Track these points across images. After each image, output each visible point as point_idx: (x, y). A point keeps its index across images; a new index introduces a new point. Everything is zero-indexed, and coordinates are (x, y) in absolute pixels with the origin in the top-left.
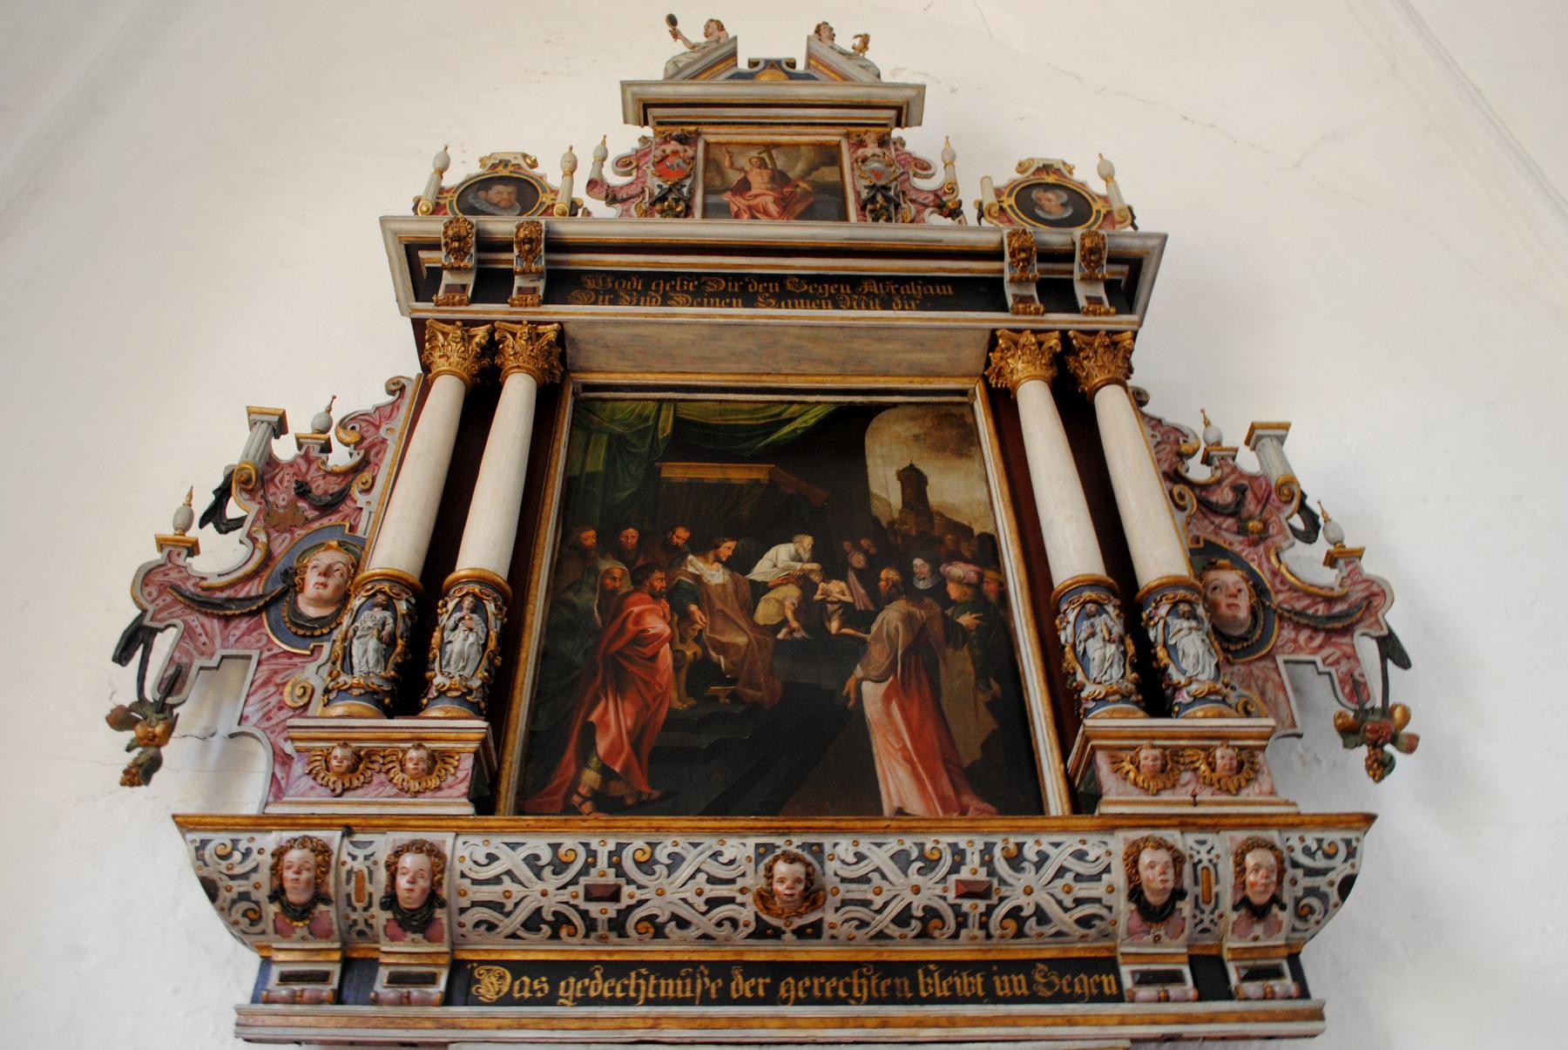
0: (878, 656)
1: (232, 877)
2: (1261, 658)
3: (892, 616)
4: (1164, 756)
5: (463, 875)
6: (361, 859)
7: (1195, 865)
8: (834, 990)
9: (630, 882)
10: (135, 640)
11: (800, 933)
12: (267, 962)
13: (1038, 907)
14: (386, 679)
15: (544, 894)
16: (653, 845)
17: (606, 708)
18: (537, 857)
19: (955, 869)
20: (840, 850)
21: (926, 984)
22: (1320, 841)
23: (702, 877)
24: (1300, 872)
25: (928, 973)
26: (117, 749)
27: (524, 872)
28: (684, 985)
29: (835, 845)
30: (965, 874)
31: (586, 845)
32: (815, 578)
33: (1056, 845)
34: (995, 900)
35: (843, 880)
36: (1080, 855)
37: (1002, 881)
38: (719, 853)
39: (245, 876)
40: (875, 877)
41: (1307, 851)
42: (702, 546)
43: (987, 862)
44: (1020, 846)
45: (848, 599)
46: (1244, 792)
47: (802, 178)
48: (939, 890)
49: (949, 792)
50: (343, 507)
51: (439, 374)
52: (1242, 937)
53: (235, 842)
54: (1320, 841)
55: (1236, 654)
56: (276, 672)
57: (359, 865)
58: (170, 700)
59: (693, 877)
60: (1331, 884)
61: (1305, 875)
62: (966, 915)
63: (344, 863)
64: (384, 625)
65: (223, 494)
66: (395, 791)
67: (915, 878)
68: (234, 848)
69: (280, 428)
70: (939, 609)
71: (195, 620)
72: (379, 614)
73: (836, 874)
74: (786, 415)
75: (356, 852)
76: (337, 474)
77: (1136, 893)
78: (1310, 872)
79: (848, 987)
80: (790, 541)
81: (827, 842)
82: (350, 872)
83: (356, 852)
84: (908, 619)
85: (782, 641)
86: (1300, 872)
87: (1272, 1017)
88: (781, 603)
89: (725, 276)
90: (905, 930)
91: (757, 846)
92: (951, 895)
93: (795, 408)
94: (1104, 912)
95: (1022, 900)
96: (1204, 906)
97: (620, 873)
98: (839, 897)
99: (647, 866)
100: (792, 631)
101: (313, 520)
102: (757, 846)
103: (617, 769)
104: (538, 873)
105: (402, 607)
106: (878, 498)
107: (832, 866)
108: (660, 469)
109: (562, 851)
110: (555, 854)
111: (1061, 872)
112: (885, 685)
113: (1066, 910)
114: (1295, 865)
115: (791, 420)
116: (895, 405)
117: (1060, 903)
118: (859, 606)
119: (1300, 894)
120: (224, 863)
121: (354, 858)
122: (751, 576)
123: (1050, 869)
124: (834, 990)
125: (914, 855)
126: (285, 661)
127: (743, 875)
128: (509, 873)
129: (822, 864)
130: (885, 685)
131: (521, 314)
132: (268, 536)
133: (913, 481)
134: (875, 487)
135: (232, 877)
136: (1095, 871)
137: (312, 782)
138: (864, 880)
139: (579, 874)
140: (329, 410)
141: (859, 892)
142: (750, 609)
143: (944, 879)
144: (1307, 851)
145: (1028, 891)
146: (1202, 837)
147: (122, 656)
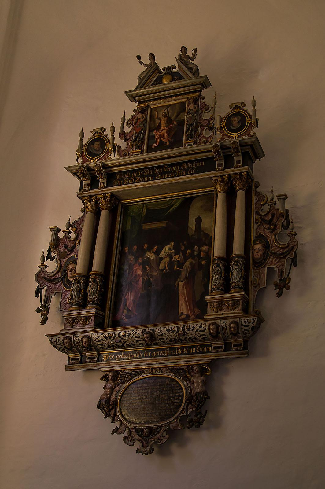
0: (183, 274)
1: (58, 345)
2: (262, 268)
3: (188, 263)
4: (219, 304)
5: (94, 340)
6: (77, 339)
7: (222, 327)
8: (162, 354)
9: (122, 339)
10: (38, 292)
11: (154, 344)
12: (69, 358)
13: (194, 337)
14: (80, 300)
15: (109, 342)
16: (125, 332)
17: (129, 295)
18: (106, 336)
19: (178, 332)
20: (157, 330)
21: (178, 351)
22: (248, 320)
23: (134, 337)
24: (243, 326)
25: (178, 349)
26: (39, 317)
27: (104, 339)
28: (137, 355)
29: (157, 329)
30: (180, 332)
31: (114, 333)
32: (173, 254)
33: (196, 325)
34: (186, 336)
35: (158, 335)
36: (201, 327)
37: (186, 333)
38: (137, 332)
39: (60, 344)
40: (164, 334)
41: (245, 322)
42: (150, 249)
43: (183, 330)
44: (190, 326)
45: (179, 260)
46: (235, 310)
47: (175, 119)
48: (175, 335)
49: (192, 308)
50: (75, 250)
51: (87, 212)
52: (234, 339)
53: (57, 338)
54: (248, 320)
55: (257, 267)
56: (65, 295)
57: (77, 340)
58: (47, 305)
59: (133, 337)
60: (249, 328)
61: (244, 327)
62: (182, 339)
63: (75, 340)
64: (78, 287)
65: (49, 251)
66: (81, 325)
67: (171, 334)
68: (57, 340)
69: (58, 230)
70: (198, 260)
71: (49, 284)
72: (77, 285)
73: (157, 334)
74: (172, 203)
75: (76, 338)
76: (72, 241)
77: (210, 334)
78: (245, 326)
79: (164, 353)
80: (169, 244)
81: (155, 328)
82: (76, 342)
83: (76, 338)
84: (191, 263)
85: (165, 273)
86: (243, 326)
87: (238, 354)
88: (165, 263)
89: (148, 168)
90: (172, 342)
91: (143, 330)
92: (178, 336)
93: (175, 200)
94: (206, 337)
95: (191, 336)
96: (225, 334)
97: (120, 337)
98: (158, 338)
99: (124, 336)
100: (167, 270)
101: (69, 255)
102: (143, 330)
103: (130, 309)
104: (107, 339)
105: (82, 282)
106: (190, 228)
107: (156, 333)
108: (142, 226)
109: (110, 335)
110: (109, 335)
111: (197, 330)
112: (183, 282)
113: (199, 337)
114: (242, 325)
115: (173, 205)
116: (198, 196)
117: (198, 336)
118: (181, 262)
119: (243, 330)
120: (56, 342)
121: (76, 339)
122: (159, 256)
123: (195, 330)
124: (162, 354)
125: (170, 329)
126: (67, 292)
127: (141, 336)
128: (102, 339)
129: (154, 333)
130: (183, 282)
131: (103, 191)
132: (60, 261)
133: (199, 221)
134: (190, 226)
135: (58, 345)
136: (203, 330)
137: (68, 325)
138: (162, 335)
139: (113, 338)
140: (69, 222)
141: (161, 337)
142: (158, 265)
143: (176, 334)
144: (245, 322)
145: (192, 334)
146: (224, 321)
147: (37, 295)
